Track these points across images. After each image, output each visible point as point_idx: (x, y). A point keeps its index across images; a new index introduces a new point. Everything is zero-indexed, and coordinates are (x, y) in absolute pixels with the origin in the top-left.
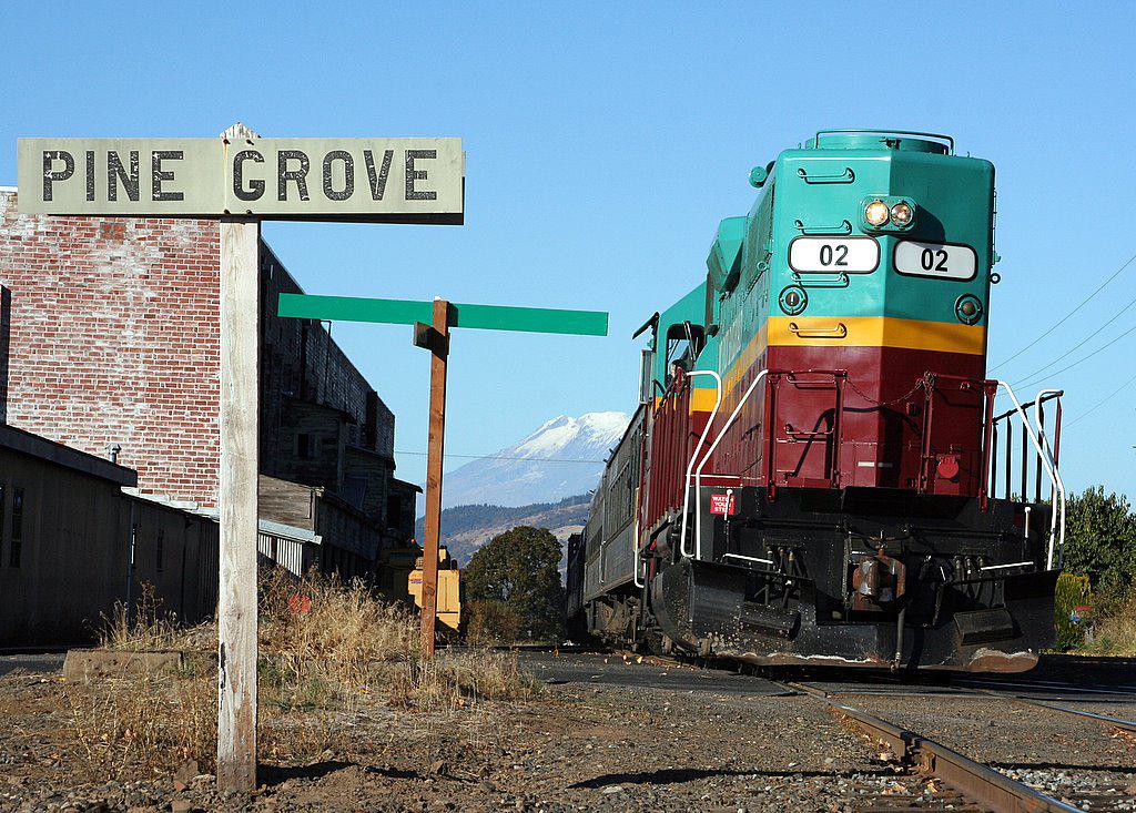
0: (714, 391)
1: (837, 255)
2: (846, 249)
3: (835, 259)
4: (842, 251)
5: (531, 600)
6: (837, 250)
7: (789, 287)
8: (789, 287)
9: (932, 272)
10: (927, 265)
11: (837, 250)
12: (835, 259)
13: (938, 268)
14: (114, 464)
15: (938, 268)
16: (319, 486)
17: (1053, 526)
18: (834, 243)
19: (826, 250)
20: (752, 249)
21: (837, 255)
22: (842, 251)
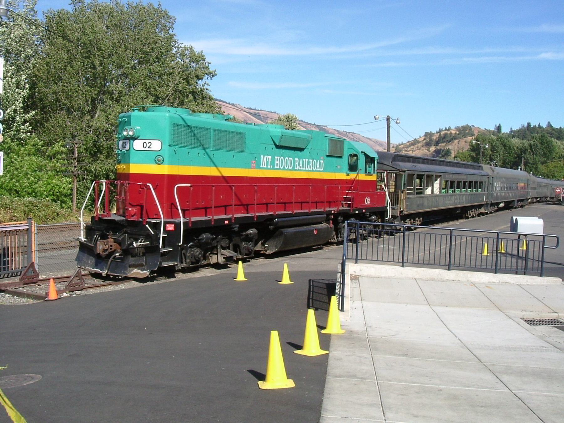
0: (510, 231)
1: (148, 145)
2: (151, 143)
3: (148, 146)
4: (150, 144)
5: (62, 78)
6: (148, 143)
7: (160, 156)
8: (160, 156)
9: (147, 149)
10: (145, 147)
11: (148, 143)
12: (148, 146)
13: (149, 148)
14: (377, 185)
15: (149, 148)
16: (429, 196)
17: (31, 301)
18: (147, 141)
19: (145, 144)
20: (423, 197)
21: (148, 145)
22: (150, 144)
